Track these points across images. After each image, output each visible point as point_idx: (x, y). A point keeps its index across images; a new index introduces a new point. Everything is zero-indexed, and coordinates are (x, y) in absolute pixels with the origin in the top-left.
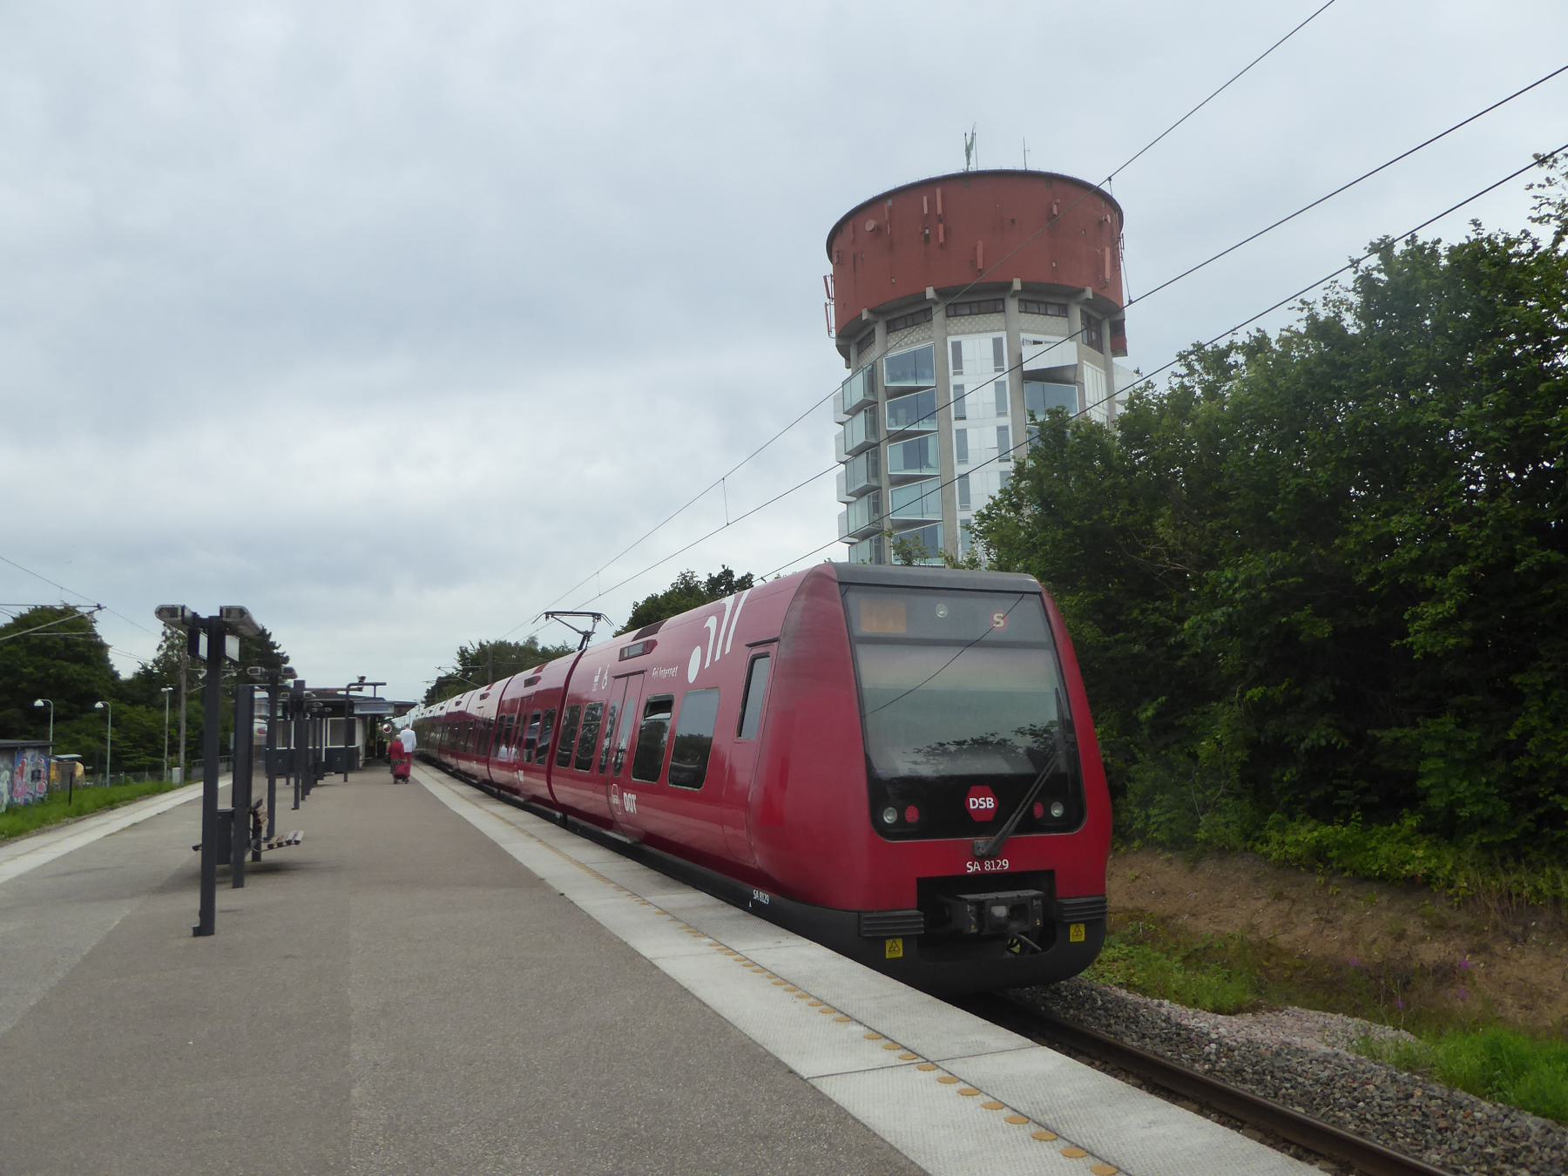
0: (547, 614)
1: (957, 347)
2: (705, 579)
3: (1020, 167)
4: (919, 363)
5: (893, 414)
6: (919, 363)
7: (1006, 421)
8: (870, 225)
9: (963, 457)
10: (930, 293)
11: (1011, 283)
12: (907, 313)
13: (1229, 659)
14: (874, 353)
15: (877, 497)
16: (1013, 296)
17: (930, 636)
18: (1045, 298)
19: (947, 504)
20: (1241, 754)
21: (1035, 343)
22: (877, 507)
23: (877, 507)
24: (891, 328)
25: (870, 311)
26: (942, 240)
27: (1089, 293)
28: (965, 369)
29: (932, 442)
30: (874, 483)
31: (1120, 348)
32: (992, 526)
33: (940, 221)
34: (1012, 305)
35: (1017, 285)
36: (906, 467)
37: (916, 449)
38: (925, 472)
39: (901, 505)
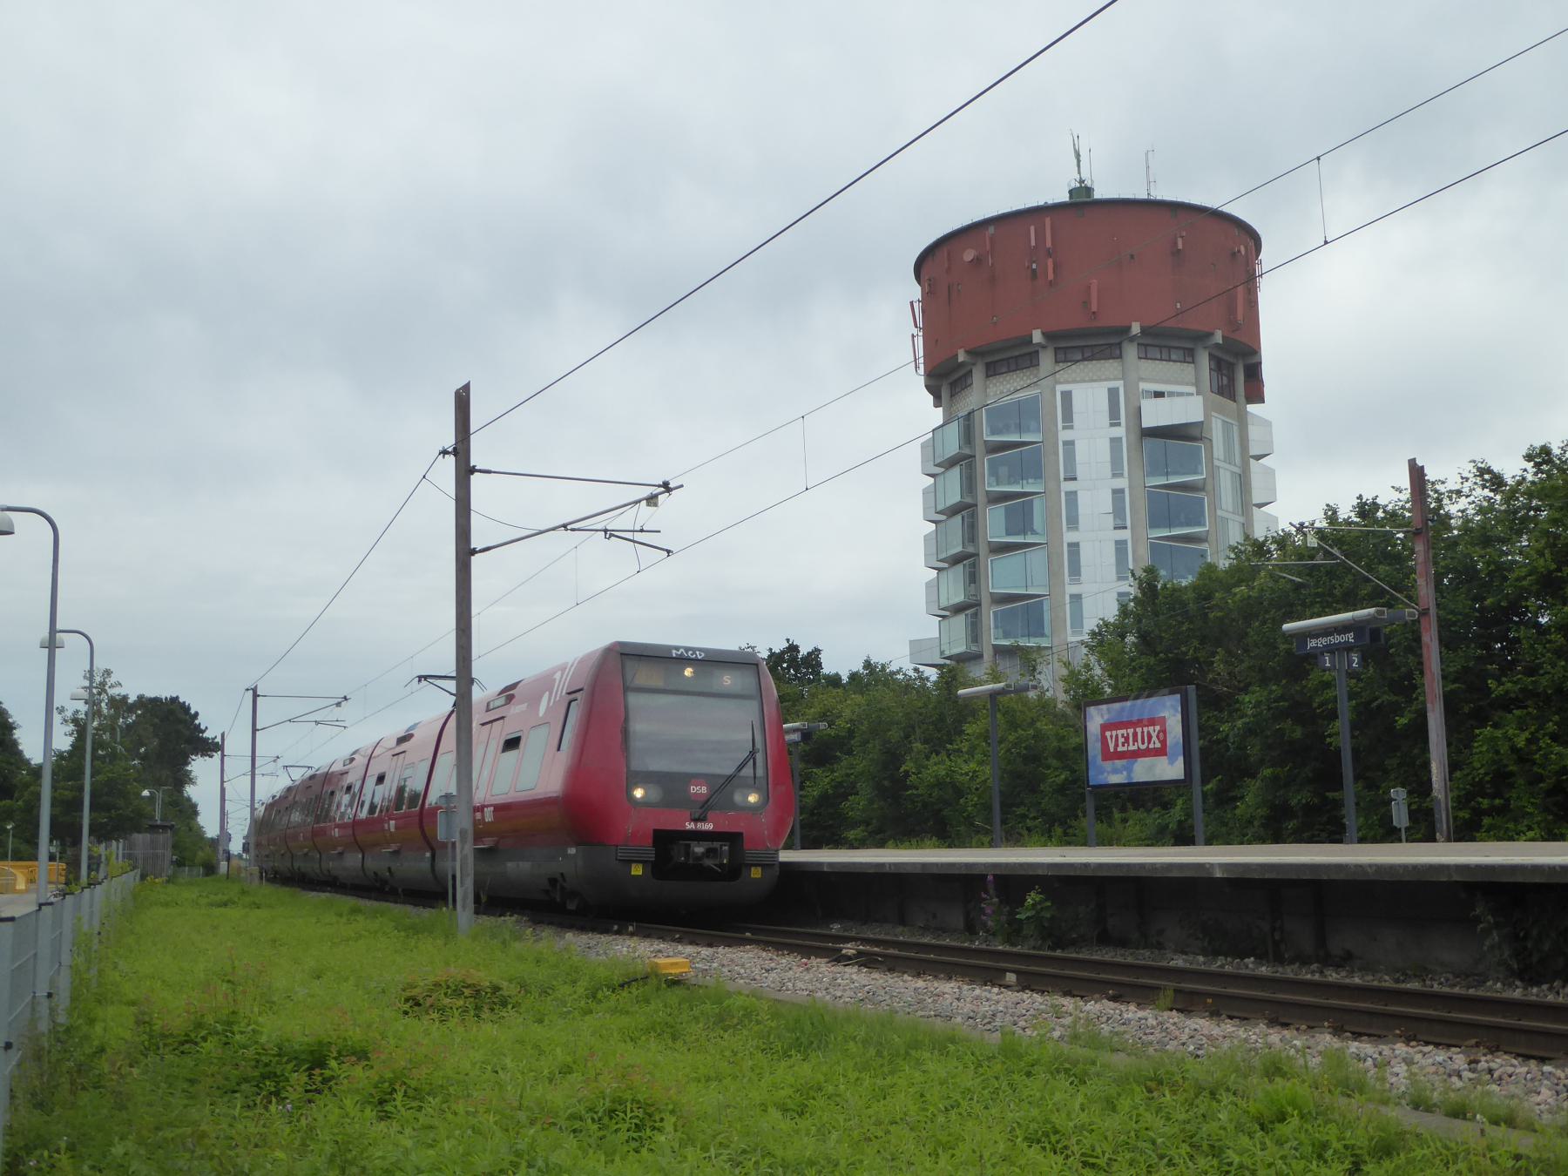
0: (420, 678)
1: (1067, 396)
2: (765, 654)
3: (1143, 195)
4: (1025, 414)
5: (994, 472)
6: (1025, 414)
7: (1122, 483)
8: (969, 255)
9: (1073, 522)
10: (1037, 337)
11: (1129, 328)
12: (1009, 356)
13: (1254, 749)
14: (971, 400)
15: (973, 565)
16: (1132, 339)
17: (694, 698)
18: (1168, 342)
19: (1053, 573)
20: (1262, 812)
21: (1159, 395)
22: (973, 578)
23: (973, 578)
24: (992, 371)
25: (968, 352)
26: (1051, 276)
27: (1218, 338)
28: (1084, 577)
29: (1037, 505)
30: (971, 549)
31: (1255, 393)
32: (1102, 640)
33: (1049, 255)
34: (1131, 351)
35: (1136, 329)
36: (1008, 534)
37: (1019, 509)
38: (1030, 539)
39: (1002, 576)
